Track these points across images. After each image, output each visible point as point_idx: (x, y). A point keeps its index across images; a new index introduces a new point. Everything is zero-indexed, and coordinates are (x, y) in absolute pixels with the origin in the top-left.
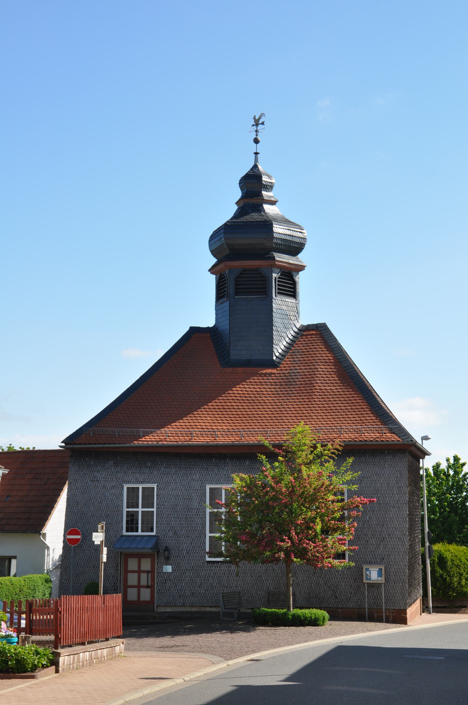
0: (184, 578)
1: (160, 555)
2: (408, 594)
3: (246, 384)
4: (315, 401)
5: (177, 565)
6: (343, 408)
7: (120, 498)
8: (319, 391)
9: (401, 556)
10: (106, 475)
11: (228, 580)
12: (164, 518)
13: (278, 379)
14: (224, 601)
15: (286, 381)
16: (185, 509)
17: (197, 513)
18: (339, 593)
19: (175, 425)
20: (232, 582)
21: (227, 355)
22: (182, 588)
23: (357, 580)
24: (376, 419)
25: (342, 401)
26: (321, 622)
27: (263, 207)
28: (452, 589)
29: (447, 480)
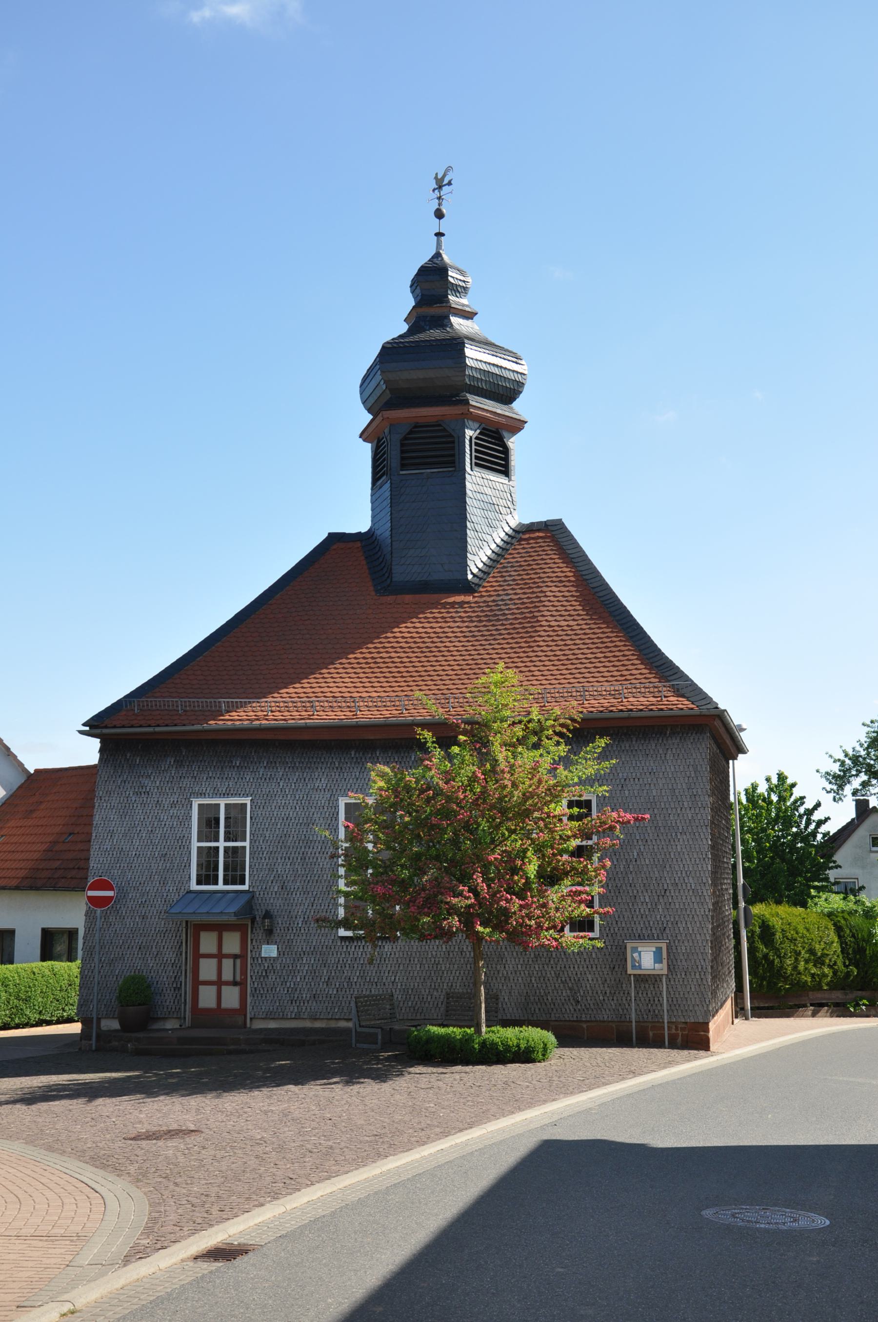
0: (298, 968)
1: (256, 925)
2: (712, 994)
3: (418, 620)
4: (538, 646)
5: (286, 944)
6: (590, 656)
7: (186, 823)
8: (547, 628)
9: (698, 923)
10: (162, 783)
11: (378, 972)
12: (263, 859)
13: (474, 612)
14: (358, 1012)
15: (489, 613)
16: (301, 842)
17: (323, 850)
18: (582, 993)
19: (287, 693)
20: (387, 974)
21: (387, 575)
22: (296, 986)
23: (616, 969)
24: (650, 673)
25: (588, 644)
26: (540, 1054)
27: (450, 320)
28: (783, 977)
29: (769, 811)
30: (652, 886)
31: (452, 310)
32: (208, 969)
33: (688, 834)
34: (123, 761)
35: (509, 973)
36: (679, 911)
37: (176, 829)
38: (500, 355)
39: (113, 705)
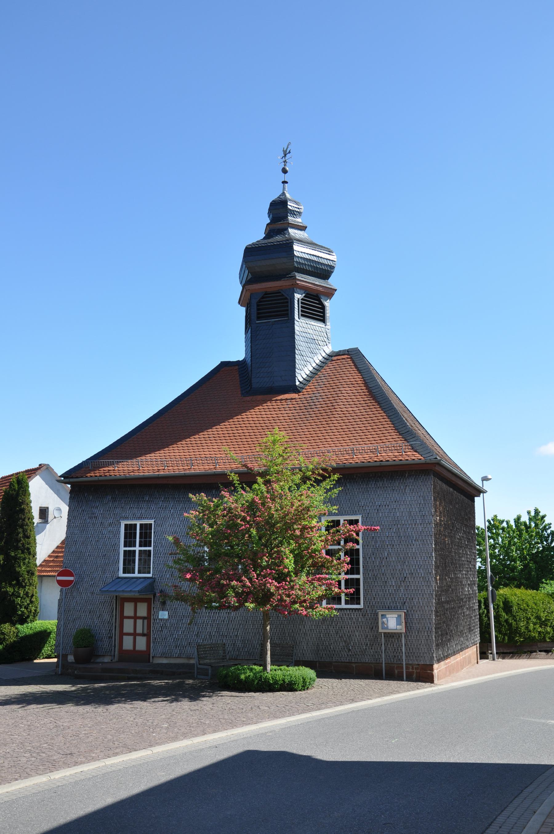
0: (180, 626)
1: (156, 599)
5: (173, 610)
7: (117, 536)
9: (426, 599)
11: (227, 629)
12: (161, 558)
20: (232, 631)
22: (179, 637)
23: (374, 629)
30: (396, 574)
31: (290, 225)
32: (128, 626)
33: (419, 541)
34: (83, 498)
35: (307, 630)
36: (414, 591)
37: (112, 539)
38: (321, 251)
39: (79, 465)
